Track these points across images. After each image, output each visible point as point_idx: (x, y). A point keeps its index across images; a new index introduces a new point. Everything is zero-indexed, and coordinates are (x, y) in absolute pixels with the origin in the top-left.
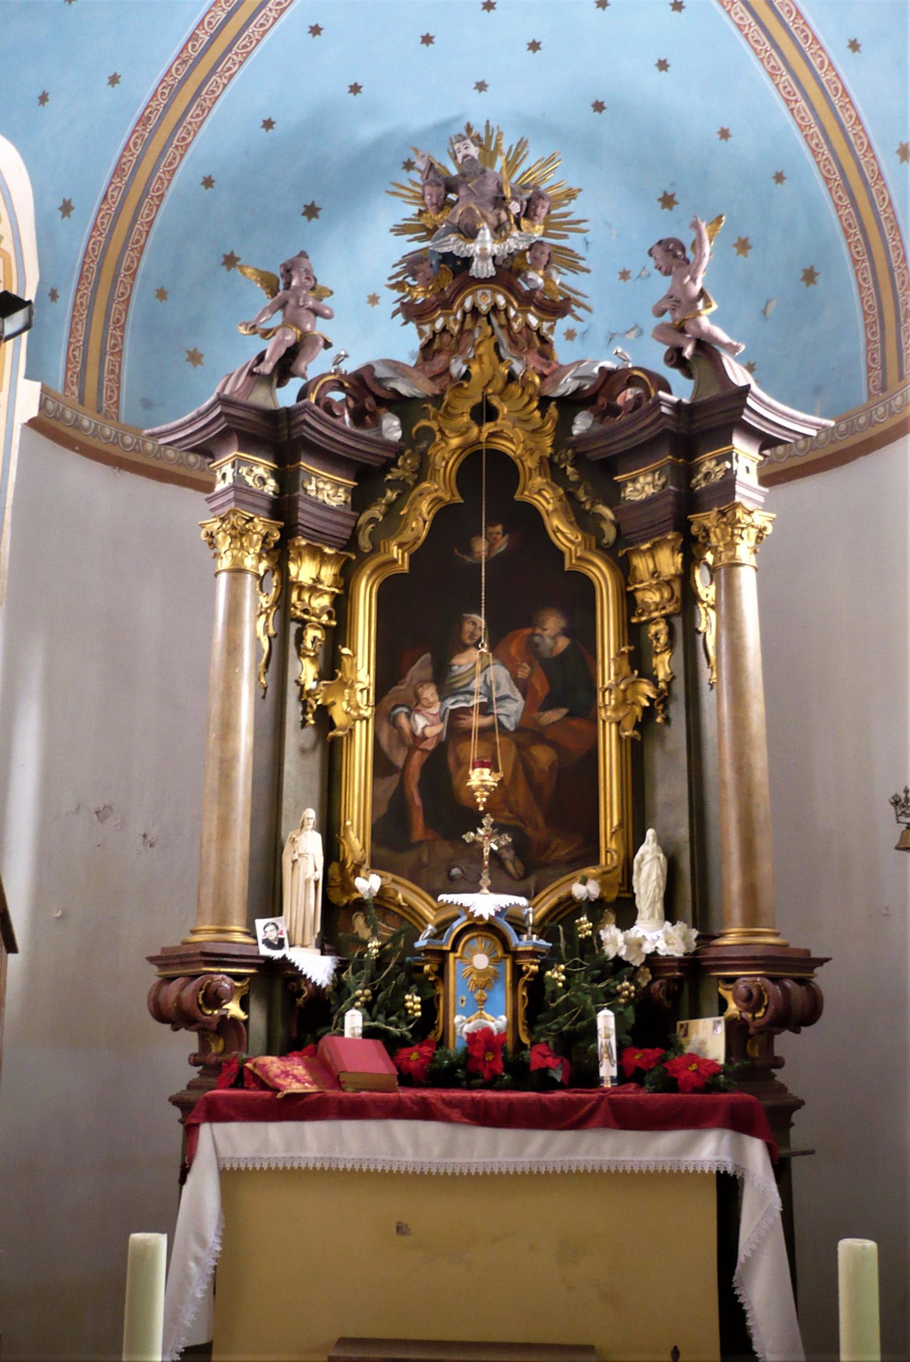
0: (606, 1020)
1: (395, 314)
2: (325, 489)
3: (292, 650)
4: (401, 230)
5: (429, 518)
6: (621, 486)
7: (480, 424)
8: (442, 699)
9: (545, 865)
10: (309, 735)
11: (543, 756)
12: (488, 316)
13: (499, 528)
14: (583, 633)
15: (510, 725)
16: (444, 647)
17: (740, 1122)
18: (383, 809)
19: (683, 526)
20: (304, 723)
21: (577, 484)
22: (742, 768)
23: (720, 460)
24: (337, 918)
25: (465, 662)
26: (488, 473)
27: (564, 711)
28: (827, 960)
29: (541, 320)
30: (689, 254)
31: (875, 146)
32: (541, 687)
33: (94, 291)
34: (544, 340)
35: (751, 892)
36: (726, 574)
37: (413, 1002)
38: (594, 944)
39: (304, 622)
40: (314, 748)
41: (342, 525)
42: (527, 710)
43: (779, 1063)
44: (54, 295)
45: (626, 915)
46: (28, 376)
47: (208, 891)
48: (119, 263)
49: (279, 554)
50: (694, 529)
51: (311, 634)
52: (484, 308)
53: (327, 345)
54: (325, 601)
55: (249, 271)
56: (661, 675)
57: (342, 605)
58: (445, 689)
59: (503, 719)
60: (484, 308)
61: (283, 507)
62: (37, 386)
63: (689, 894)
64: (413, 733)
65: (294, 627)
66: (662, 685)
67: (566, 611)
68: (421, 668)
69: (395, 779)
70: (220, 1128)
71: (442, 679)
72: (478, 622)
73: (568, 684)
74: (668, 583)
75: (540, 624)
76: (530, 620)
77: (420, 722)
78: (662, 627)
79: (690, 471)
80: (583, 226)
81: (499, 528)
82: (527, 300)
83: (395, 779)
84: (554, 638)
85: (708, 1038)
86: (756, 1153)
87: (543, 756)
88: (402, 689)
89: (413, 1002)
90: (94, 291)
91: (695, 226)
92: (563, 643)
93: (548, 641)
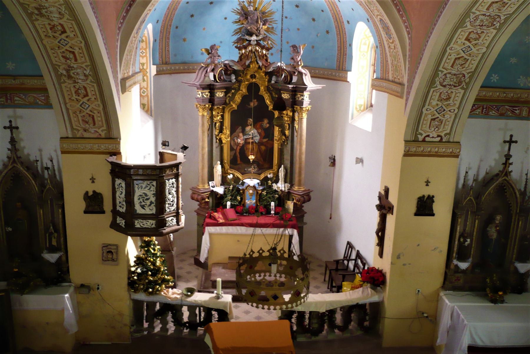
0: (273, 204)
2: (220, 94)
3: (214, 128)
9: (263, 169)
10: (217, 144)
11: (263, 148)
15: (257, 142)
16: (244, 126)
17: (293, 227)
18: (232, 157)
20: (217, 142)
22: (300, 158)
24: (224, 182)
25: (248, 128)
26: (253, 88)
32: (263, 134)
34: (266, 56)
35: (300, 181)
37: (239, 198)
38: (270, 187)
42: (260, 139)
46: (153, 64)
47: (200, 179)
51: (217, 124)
58: (244, 134)
60: (253, 50)
61: (211, 100)
63: (289, 179)
65: (214, 124)
69: (234, 152)
70: (208, 227)
71: (244, 132)
72: (251, 120)
73: (268, 134)
75: (263, 121)
77: (239, 140)
78: (287, 125)
80: (276, 22)
82: (263, 47)
83: (234, 152)
85: (290, 205)
86: (295, 232)
87: (263, 148)
88: (235, 134)
89: (239, 198)
92: (268, 125)
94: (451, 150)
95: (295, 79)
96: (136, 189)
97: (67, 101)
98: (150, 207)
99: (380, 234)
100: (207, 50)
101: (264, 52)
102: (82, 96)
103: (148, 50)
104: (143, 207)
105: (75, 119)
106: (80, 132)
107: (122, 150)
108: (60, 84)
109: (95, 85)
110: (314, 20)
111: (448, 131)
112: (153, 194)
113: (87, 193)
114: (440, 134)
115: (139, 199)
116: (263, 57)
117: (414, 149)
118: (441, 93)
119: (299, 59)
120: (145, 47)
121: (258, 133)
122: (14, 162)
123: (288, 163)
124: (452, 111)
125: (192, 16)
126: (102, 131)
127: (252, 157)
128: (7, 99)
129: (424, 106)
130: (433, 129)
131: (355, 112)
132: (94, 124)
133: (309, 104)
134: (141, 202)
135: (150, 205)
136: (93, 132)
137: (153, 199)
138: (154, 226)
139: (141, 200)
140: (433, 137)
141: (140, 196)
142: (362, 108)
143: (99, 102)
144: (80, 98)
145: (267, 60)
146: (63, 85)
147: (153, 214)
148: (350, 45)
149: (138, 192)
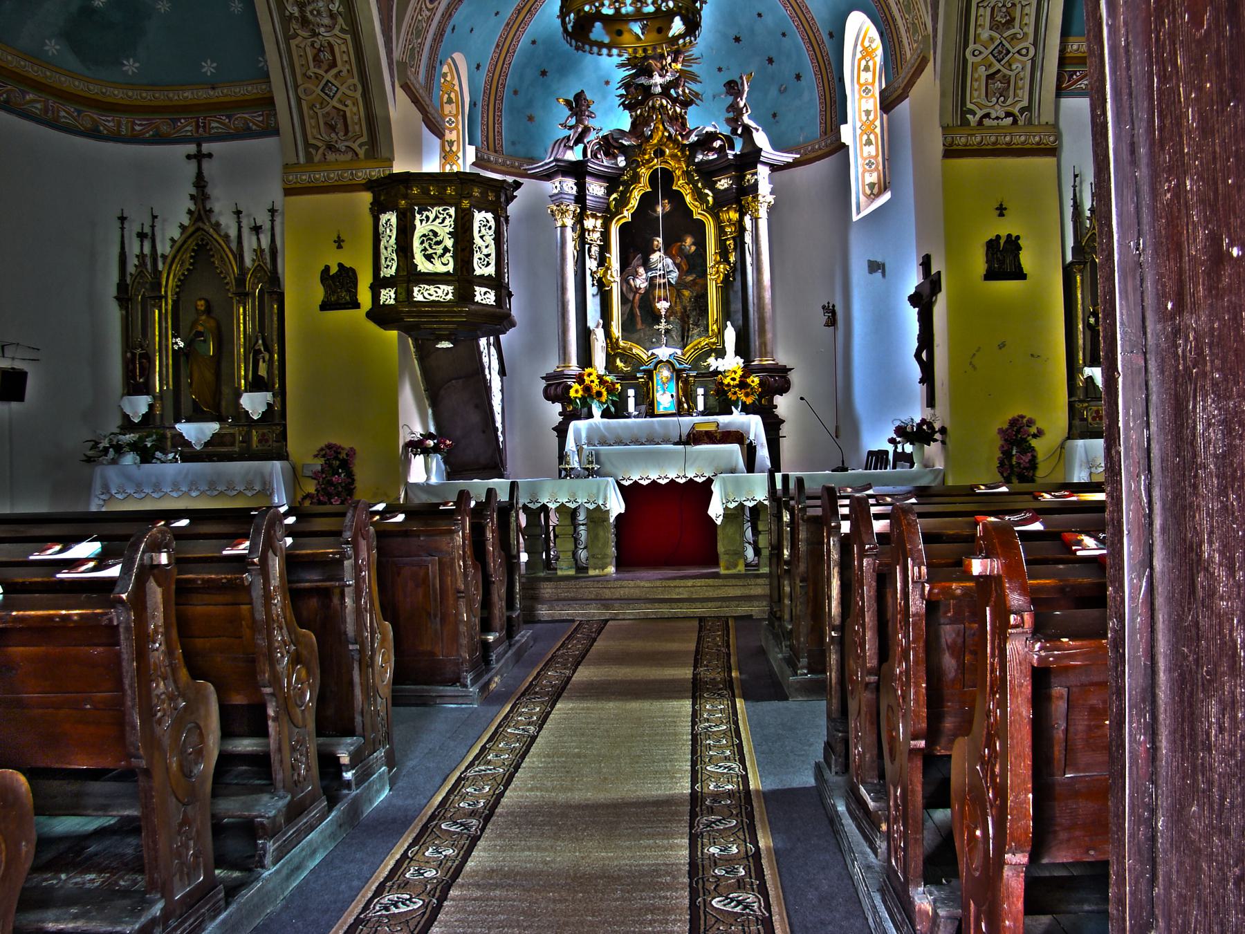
2: (596, 189)
4: (621, 65)
6: (716, 182)
14: (701, 243)
19: (739, 202)
22: (760, 297)
23: (753, 174)
25: (655, 257)
34: (683, 118)
36: (755, 220)
42: (680, 277)
43: (776, 407)
45: (721, 354)
49: (579, 219)
54: (598, 235)
57: (605, 235)
58: (648, 268)
61: (581, 198)
62: (473, 148)
67: (693, 236)
73: (694, 265)
77: (638, 282)
91: (741, 78)
92: (693, 248)
94: (1037, 139)
96: (417, 222)
97: (300, 81)
98: (444, 260)
99: (924, 355)
100: (568, 103)
101: (678, 110)
102: (325, 67)
104: (429, 258)
105: (313, 122)
106: (321, 151)
108: (288, 39)
109: (348, 37)
110: (770, 61)
111: (1025, 103)
112: (450, 233)
113: (327, 268)
114: (1010, 109)
115: (422, 243)
116: (677, 120)
117: (963, 140)
118: (993, 9)
119: (742, 104)
121: (674, 263)
122: (199, 219)
123: (739, 317)
124: (1024, 52)
125: (544, 73)
126: (360, 146)
127: (663, 306)
128: (198, 126)
129: (966, 45)
130: (994, 99)
131: (862, 198)
132: (346, 133)
133: (771, 193)
134: (425, 249)
135: (442, 255)
136: (343, 149)
137: (449, 243)
138: (450, 297)
140: (997, 118)
141: (424, 235)
142: (876, 190)
143: (356, 81)
144: (321, 72)
145: (684, 125)
146: (293, 43)
147: (448, 273)
149: (421, 229)
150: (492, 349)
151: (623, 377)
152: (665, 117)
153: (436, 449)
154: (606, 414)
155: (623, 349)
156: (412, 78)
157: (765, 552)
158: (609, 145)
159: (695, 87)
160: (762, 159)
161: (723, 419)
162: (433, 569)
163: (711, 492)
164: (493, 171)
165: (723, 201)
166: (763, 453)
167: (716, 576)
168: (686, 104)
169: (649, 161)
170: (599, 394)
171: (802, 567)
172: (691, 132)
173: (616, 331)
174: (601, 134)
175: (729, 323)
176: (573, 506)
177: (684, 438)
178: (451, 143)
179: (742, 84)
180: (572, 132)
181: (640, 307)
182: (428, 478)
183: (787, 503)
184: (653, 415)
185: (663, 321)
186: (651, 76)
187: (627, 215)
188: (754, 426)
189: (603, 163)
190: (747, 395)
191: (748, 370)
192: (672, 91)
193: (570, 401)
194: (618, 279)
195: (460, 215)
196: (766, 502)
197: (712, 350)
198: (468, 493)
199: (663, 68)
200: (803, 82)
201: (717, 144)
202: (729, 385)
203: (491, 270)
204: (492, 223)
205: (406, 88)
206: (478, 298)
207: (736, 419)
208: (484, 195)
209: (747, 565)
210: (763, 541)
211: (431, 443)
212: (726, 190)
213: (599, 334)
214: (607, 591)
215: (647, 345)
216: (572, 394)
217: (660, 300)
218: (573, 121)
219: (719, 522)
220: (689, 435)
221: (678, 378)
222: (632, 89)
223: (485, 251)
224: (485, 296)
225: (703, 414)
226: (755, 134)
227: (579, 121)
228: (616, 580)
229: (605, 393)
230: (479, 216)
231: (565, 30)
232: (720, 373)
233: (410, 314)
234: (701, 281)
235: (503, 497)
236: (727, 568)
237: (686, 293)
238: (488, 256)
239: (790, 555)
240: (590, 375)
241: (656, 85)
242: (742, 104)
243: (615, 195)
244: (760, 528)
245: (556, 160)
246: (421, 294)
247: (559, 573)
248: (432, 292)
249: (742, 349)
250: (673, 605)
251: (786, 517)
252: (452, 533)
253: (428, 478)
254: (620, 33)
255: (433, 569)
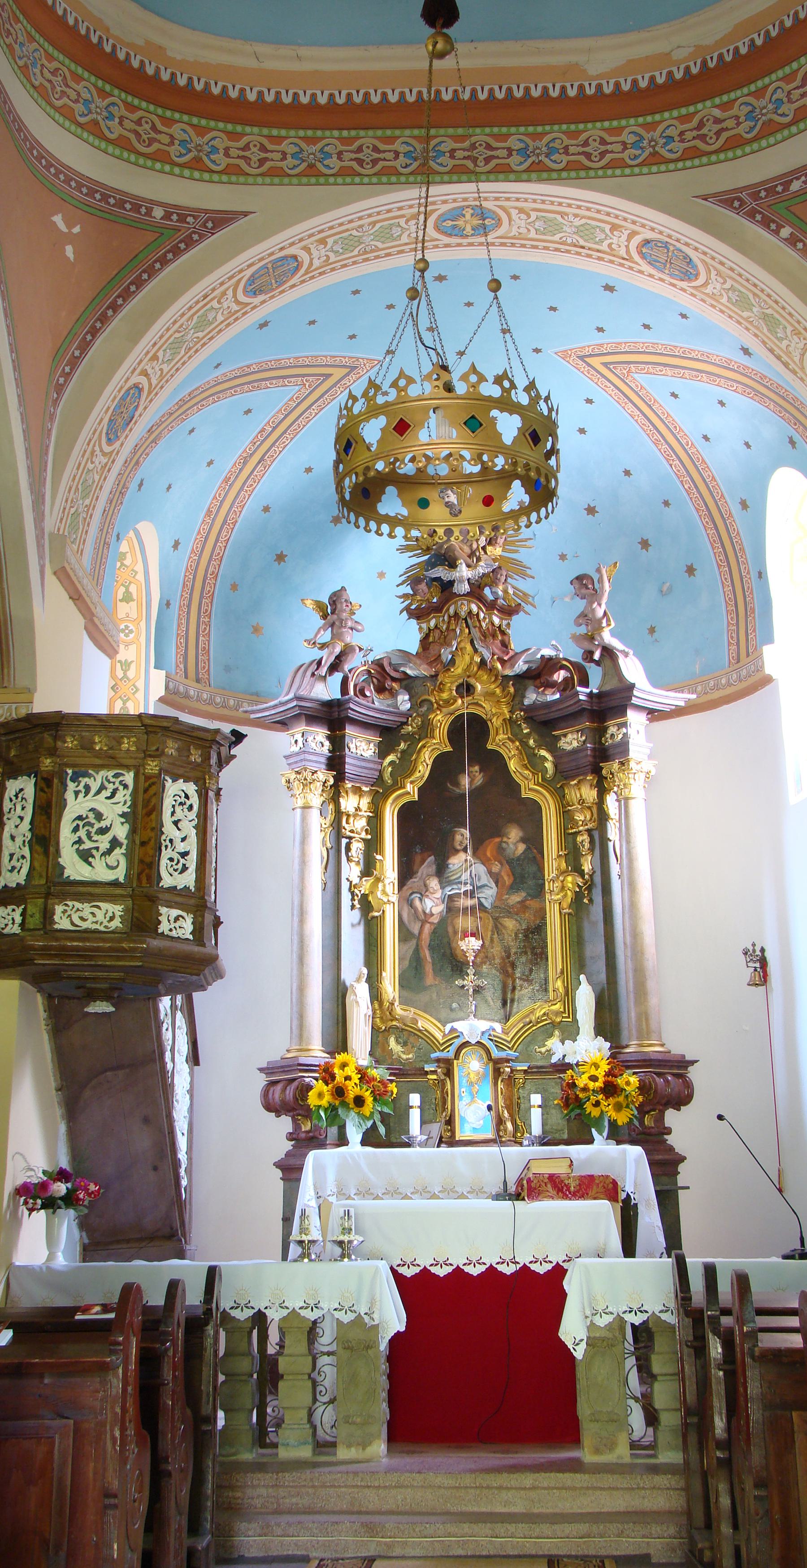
1: (401, 612)
2: (361, 746)
5: (430, 762)
6: (557, 738)
7: (462, 697)
8: (442, 888)
10: (356, 915)
12: (465, 619)
13: (477, 768)
14: (534, 841)
15: (487, 904)
16: (442, 852)
21: (528, 735)
25: (456, 862)
26: (470, 733)
27: (524, 894)
28: (696, 1061)
29: (501, 619)
30: (597, 586)
31: (725, 495)
32: (507, 880)
33: (191, 595)
34: (503, 633)
36: (624, 802)
39: (350, 838)
40: (359, 923)
41: (371, 769)
42: (499, 896)
43: (669, 1131)
44: (168, 604)
48: (206, 571)
49: (335, 793)
50: (604, 772)
52: (463, 614)
53: (361, 649)
55: (308, 602)
56: (586, 871)
57: (375, 822)
59: (483, 900)
60: (463, 614)
61: (336, 763)
62: (164, 672)
64: (424, 913)
65: (344, 841)
66: (586, 877)
67: (521, 827)
68: (429, 866)
69: (414, 942)
71: (441, 871)
72: (464, 835)
73: (526, 875)
74: (589, 808)
75: (506, 835)
76: (498, 832)
77: (429, 904)
78: (586, 837)
79: (602, 731)
81: (477, 768)
82: (491, 606)
84: (515, 844)
90: (191, 595)
91: (598, 570)
92: (522, 847)
93: (511, 846)
95: (595, 675)
96: (69, 795)
98: (111, 860)
100: (320, 606)
101: (496, 621)
103: (143, 624)
104: (86, 856)
107: (35, 701)
110: (645, 544)
112: (123, 815)
115: (76, 829)
116: (494, 636)
119: (600, 613)
120: (134, 615)
121: (490, 873)
123: (600, 967)
125: (280, 558)
127: (470, 945)
133: (650, 757)
134: (80, 841)
135: (109, 852)
137: (121, 831)
138: (116, 923)
139: (82, 833)
141: (80, 818)
145: (505, 645)
147: (115, 884)
148: (761, 575)
149: (76, 806)
150: (179, 1015)
151: (400, 1072)
152: (476, 633)
153: (70, 1200)
154: (370, 1139)
155: (402, 1020)
156: (73, 560)
157: (670, 1419)
158: (384, 677)
159: (523, 585)
160: (634, 701)
161: (577, 1151)
162: (63, 1445)
163: (563, 1295)
164: (193, 712)
165: (568, 770)
166: (650, 1219)
167: (575, 1466)
168: (509, 612)
169: (448, 703)
170: (359, 1101)
171: (757, 1456)
172: (517, 655)
173: (390, 987)
174: (371, 658)
175: (582, 977)
176: (311, 1315)
177: (512, 1189)
178: (126, 666)
179: (601, 581)
180: (324, 653)
181: (431, 948)
182: (51, 1257)
183: (714, 1321)
184: (452, 1142)
185: (471, 971)
186: (453, 565)
187: (411, 790)
188: (630, 1164)
189: (375, 705)
190: (618, 1107)
191: (619, 1061)
192: (487, 591)
193: (308, 1113)
194: (394, 898)
195: (142, 785)
196: (667, 1317)
197: (554, 1025)
198: (139, 1288)
199: (472, 554)
200: (699, 578)
201: (560, 676)
202: (585, 1089)
203: (188, 880)
204: (195, 800)
205: (63, 575)
206: (164, 927)
207: (600, 1154)
208: (184, 751)
209: (634, 1445)
210: (664, 1395)
211: (60, 1188)
212: (574, 751)
213: (360, 993)
214: (370, 1494)
215: (444, 1014)
216: (312, 1099)
217: (465, 935)
218: (326, 636)
219: (579, 1353)
220: (519, 1182)
221: (497, 1073)
222: (423, 587)
223: (181, 847)
224: (175, 923)
225: (545, 1141)
226: (621, 661)
227: (336, 636)
228: (389, 1470)
229: (369, 1100)
230: (173, 789)
231: (342, 499)
232: (569, 1066)
233: (45, 951)
234: (533, 904)
235: (194, 1296)
236: (597, 1451)
237: (510, 924)
238: (184, 855)
239: (729, 1429)
240: (344, 1066)
241: (461, 581)
242: (600, 613)
243: (391, 758)
244: (657, 1366)
245: (298, 698)
246: (68, 916)
247: (283, 1453)
248: (86, 913)
249: (607, 1023)
250: (500, 1528)
251: (716, 1349)
252: (104, 1368)
253: (51, 1257)
254: (424, 504)
255: (63, 1445)
